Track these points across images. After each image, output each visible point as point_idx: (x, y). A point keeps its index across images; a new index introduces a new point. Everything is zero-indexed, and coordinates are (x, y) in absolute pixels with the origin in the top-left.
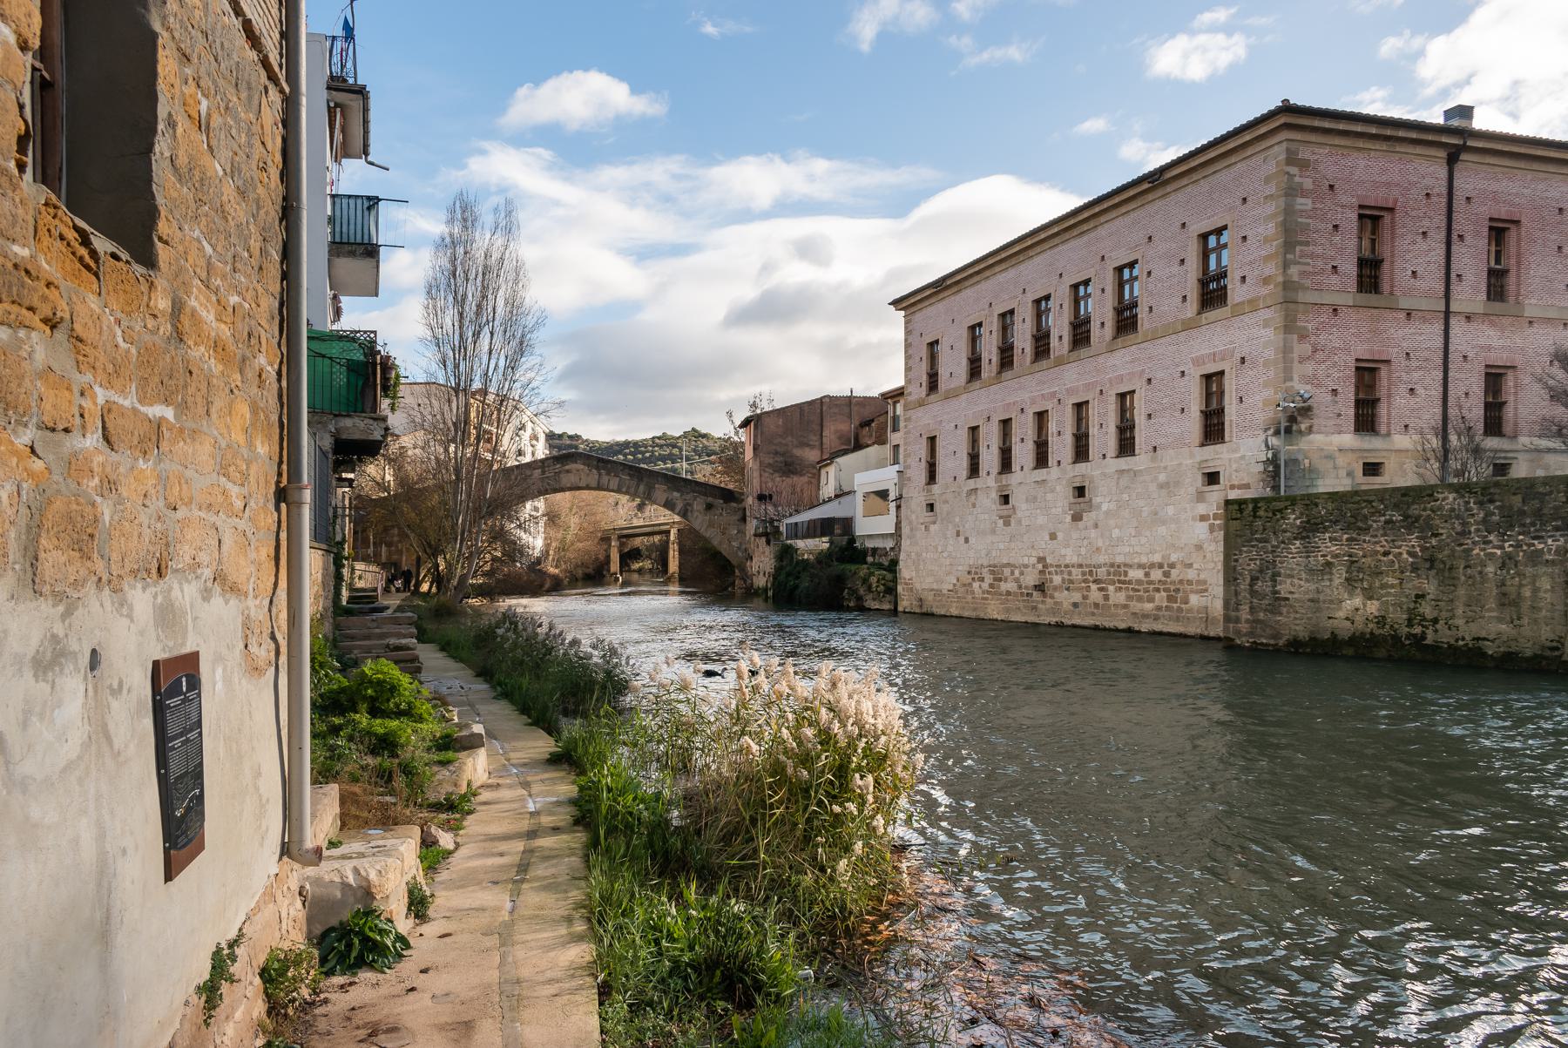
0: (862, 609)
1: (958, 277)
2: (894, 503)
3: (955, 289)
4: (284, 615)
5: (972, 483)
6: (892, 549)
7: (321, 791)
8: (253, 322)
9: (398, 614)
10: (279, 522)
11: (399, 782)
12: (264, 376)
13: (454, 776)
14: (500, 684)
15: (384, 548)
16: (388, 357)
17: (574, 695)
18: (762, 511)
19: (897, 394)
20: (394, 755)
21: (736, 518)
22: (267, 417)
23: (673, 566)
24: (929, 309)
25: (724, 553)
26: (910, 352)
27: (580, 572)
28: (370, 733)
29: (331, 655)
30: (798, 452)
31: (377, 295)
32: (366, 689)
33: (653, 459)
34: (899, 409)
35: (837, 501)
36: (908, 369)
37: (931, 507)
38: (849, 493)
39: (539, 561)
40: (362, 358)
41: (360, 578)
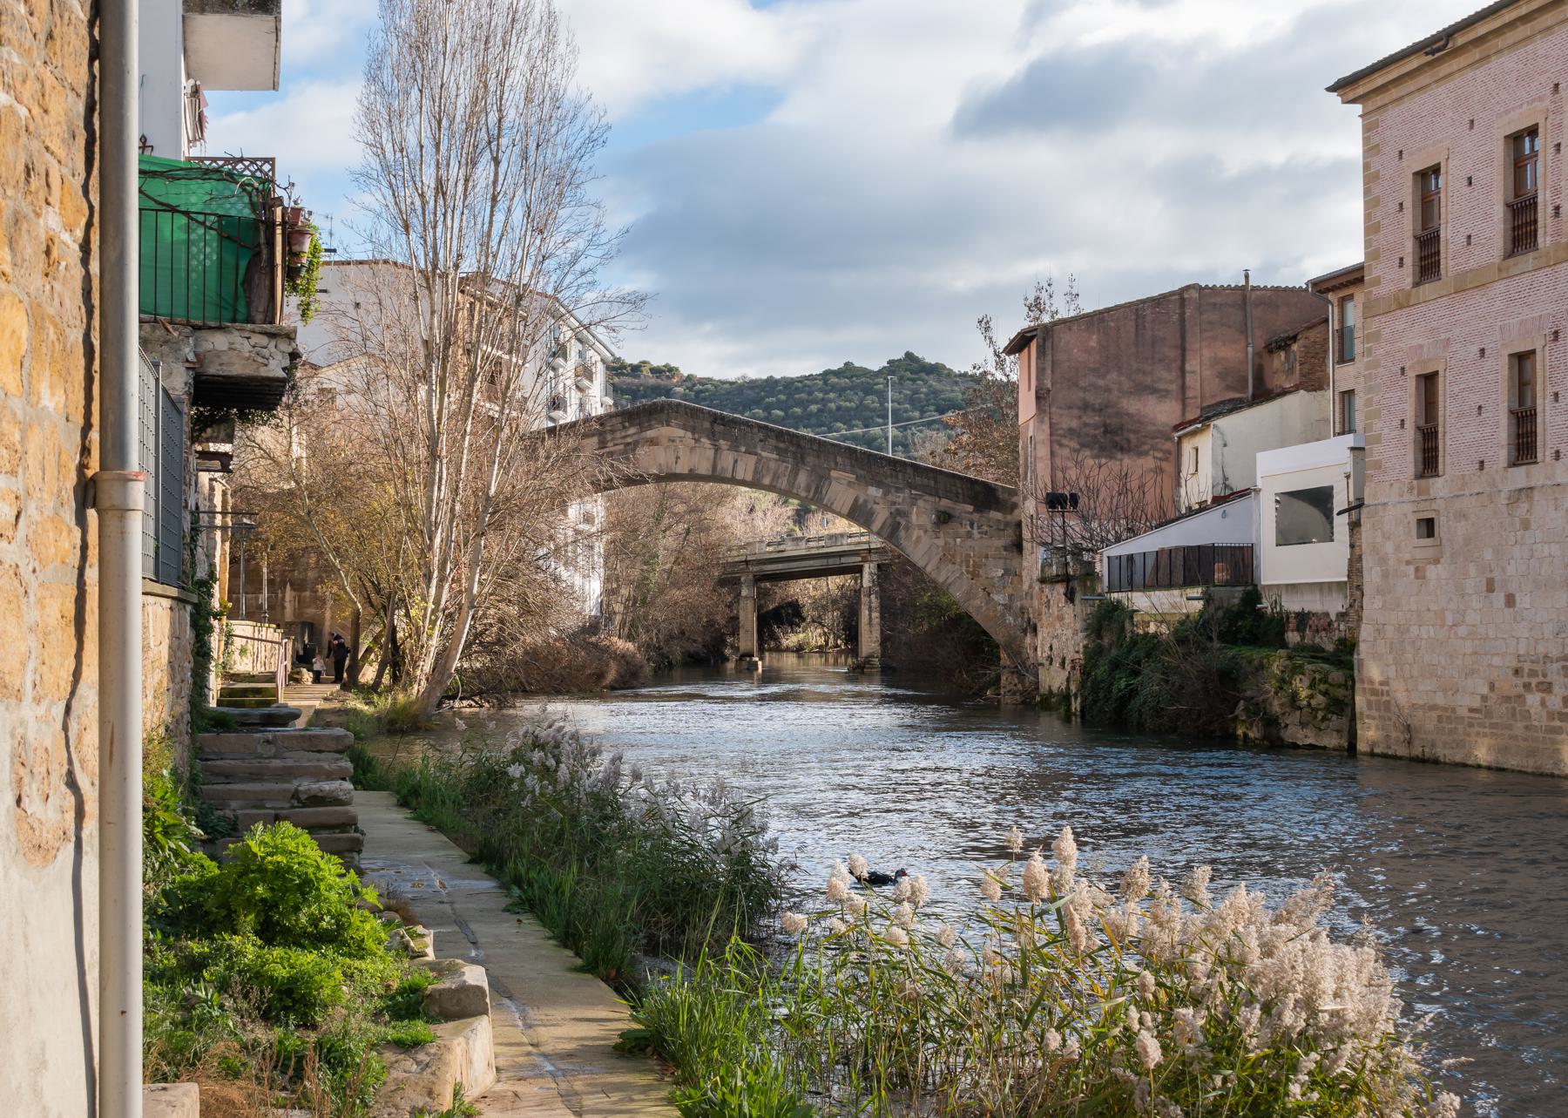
0: (1274, 745)
1: (1481, 29)
2: (1345, 518)
3: (1476, 54)
4: (92, 738)
5: (1520, 476)
6: (1342, 616)
7: (165, 1096)
8: (35, 145)
9: (317, 731)
10: (84, 547)
11: (318, 1080)
12: (55, 254)
13: (427, 1074)
14: (517, 881)
15: (289, 594)
16: (297, 211)
17: (668, 910)
18: (1058, 531)
19: (1351, 279)
20: (308, 1024)
21: (1000, 543)
22: (61, 335)
23: (870, 641)
24: (1417, 98)
25: (977, 618)
26: (1376, 191)
27: (677, 652)
28: (258, 976)
29: (185, 812)
30: (1132, 405)
31: (275, 87)
32: (253, 884)
33: (822, 419)
34: (1354, 314)
35: (1218, 511)
36: (1372, 228)
37: (1428, 527)
38: (1244, 494)
39: (593, 627)
40: (247, 213)
41: (243, 651)
